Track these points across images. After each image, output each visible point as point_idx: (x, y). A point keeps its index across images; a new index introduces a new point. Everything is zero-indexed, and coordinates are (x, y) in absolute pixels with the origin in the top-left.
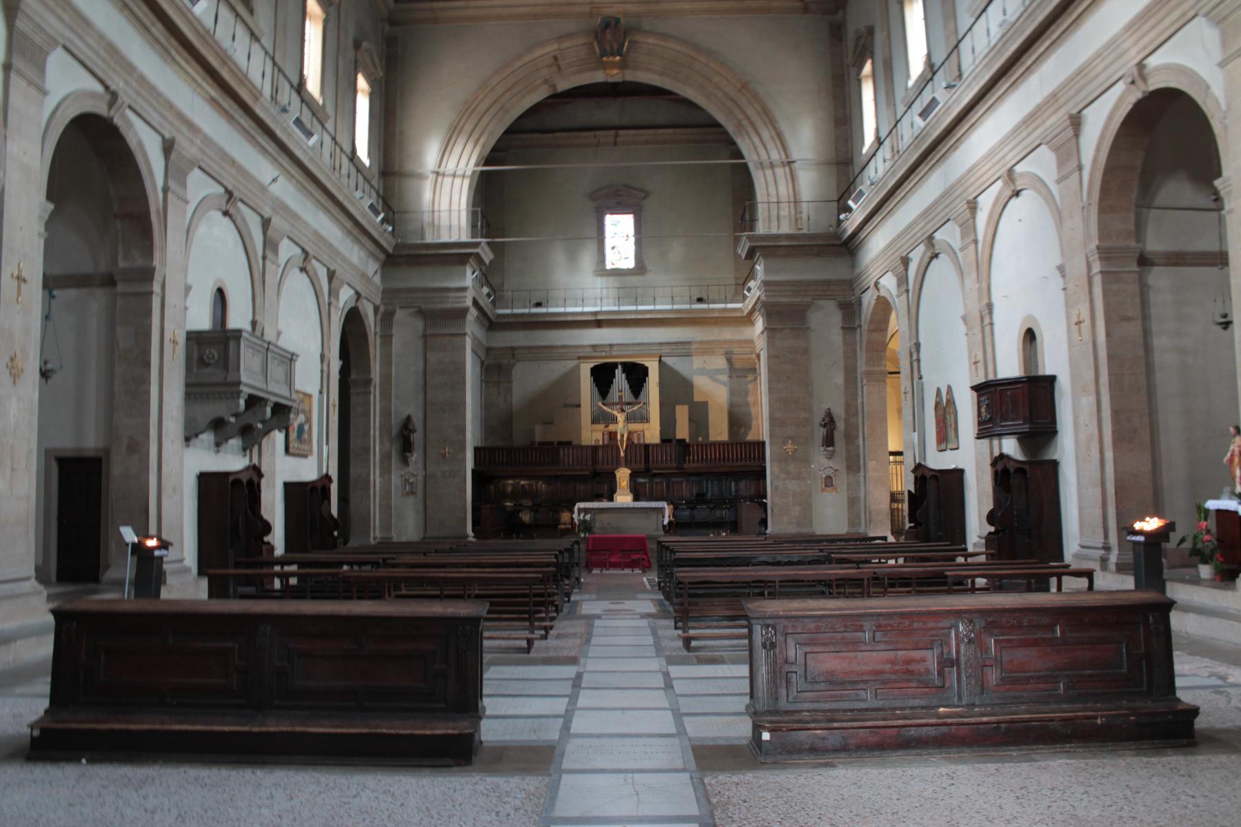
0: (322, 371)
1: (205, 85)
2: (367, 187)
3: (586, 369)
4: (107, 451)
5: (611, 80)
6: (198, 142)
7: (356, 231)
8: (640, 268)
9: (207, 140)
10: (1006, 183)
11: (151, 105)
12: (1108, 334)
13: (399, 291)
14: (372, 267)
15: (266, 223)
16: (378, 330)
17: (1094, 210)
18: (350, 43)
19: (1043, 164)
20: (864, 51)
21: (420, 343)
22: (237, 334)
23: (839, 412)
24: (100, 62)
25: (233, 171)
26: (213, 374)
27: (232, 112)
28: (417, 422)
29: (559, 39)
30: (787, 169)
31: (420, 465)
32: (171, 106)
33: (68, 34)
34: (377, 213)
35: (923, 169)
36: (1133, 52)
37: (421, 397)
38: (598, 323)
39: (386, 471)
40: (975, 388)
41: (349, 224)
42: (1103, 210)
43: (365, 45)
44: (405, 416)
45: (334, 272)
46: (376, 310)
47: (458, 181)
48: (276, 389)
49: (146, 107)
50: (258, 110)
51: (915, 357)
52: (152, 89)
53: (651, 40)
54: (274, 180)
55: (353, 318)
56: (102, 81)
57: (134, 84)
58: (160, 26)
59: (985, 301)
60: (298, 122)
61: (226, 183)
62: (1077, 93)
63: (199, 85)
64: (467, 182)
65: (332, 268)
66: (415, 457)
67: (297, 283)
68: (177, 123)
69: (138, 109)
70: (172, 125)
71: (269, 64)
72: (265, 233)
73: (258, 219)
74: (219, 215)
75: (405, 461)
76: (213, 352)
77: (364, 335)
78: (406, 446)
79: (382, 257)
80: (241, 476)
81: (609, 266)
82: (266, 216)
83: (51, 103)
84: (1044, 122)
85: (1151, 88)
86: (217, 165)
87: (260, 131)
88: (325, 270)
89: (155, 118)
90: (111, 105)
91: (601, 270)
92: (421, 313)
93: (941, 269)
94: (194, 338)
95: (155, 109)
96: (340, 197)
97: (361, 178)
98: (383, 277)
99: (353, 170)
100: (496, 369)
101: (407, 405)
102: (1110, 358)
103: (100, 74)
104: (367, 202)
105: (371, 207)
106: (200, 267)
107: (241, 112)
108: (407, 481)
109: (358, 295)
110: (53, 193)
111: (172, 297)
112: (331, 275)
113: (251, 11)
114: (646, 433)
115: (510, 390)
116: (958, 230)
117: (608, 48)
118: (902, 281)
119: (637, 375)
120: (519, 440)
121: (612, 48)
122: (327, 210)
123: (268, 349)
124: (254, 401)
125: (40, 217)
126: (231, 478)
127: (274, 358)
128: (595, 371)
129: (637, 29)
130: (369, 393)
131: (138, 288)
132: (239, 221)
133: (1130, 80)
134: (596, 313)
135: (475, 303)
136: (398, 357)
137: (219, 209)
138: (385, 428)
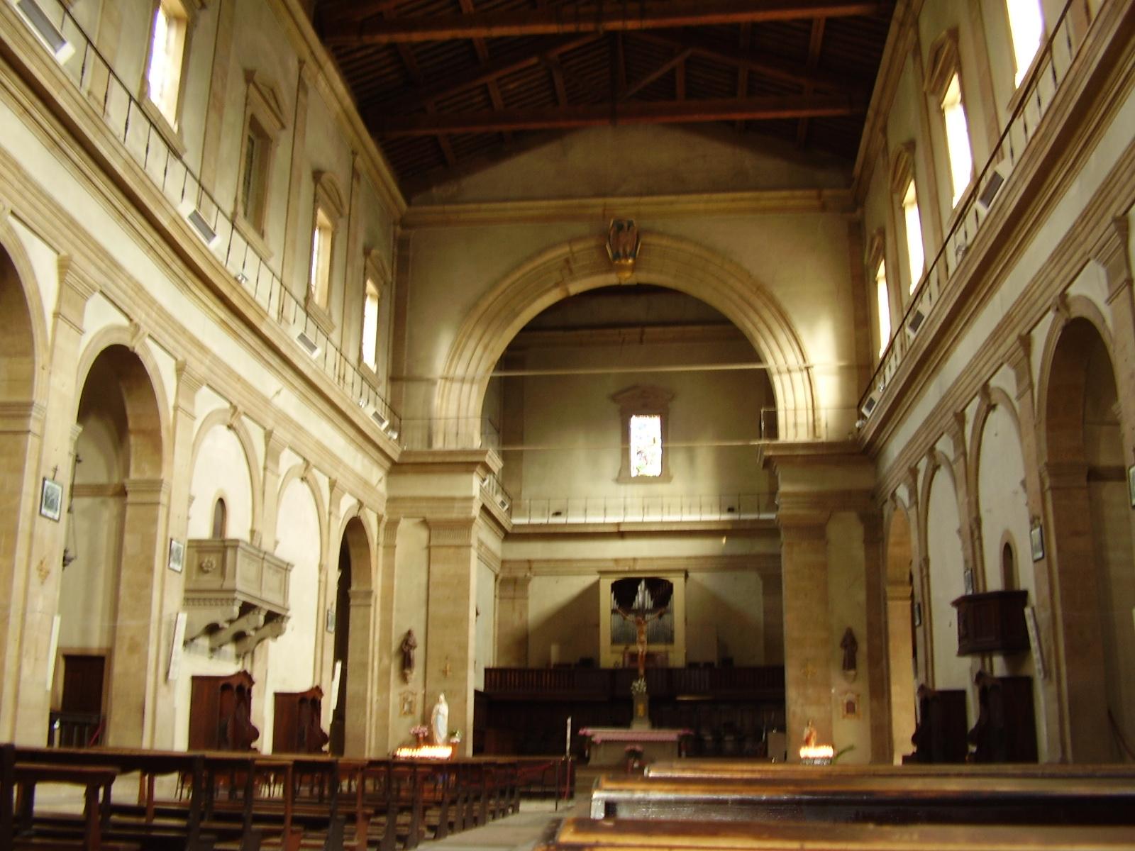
0: (320, 581)
1: (215, 309)
2: (372, 393)
3: (606, 585)
4: (111, 651)
5: (623, 283)
6: (207, 362)
7: (360, 440)
8: (665, 476)
9: (216, 360)
10: (982, 399)
11: (167, 332)
12: (1059, 549)
13: (403, 499)
14: (376, 475)
15: (268, 435)
16: (382, 539)
17: (1043, 427)
18: (360, 250)
19: (1005, 380)
20: (881, 252)
21: (424, 554)
22: (235, 544)
23: (861, 632)
24: (127, 300)
25: (239, 386)
26: (210, 581)
27: (239, 331)
28: (419, 638)
29: (571, 241)
30: (805, 373)
31: (421, 684)
32: (183, 330)
33: (103, 279)
34: (382, 421)
35: (921, 378)
36: (1058, 281)
37: (423, 611)
38: (620, 534)
39: (384, 687)
40: (957, 603)
41: (352, 432)
42: (1051, 427)
43: (374, 252)
44: (405, 630)
45: (335, 481)
46: (380, 519)
47: (466, 387)
48: (269, 597)
49: (163, 333)
50: (265, 330)
51: (925, 573)
52: (169, 318)
53: (664, 242)
54: (278, 393)
55: (355, 527)
56: (127, 315)
57: (154, 314)
58: (179, 263)
59: (974, 515)
60: (302, 337)
61: (230, 398)
62: (1025, 315)
63: (211, 310)
64: (475, 388)
65: (333, 477)
66: (416, 673)
67: (298, 494)
68: (189, 346)
69: (155, 336)
70: (184, 348)
71: (277, 285)
72: (267, 444)
73: (261, 432)
74: (224, 428)
75: (404, 678)
76: (213, 560)
77: (366, 545)
78: (406, 662)
79: (387, 464)
80: (231, 681)
81: (634, 473)
82: (268, 428)
83: (86, 340)
84: (1005, 341)
85: (1073, 316)
86: (221, 379)
87: (265, 348)
88: (327, 480)
89: (170, 343)
90: (134, 335)
91: (623, 476)
92: (425, 523)
93: (942, 480)
94: (197, 546)
95: (170, 335)
96: (343, 407)
97: (365, 386)
98: (389, 485)
99: (358, 379)
100: (511, 583)
101: (409, 618)
102: (1061, 572)
103: (126, 310)
104: (370, 410)
105: (376, 414)
106: (204, 471)
107: (248, 331)
108: (405, 700)
109: (361, 505)
110: (83, 415)
111: (178, 507)
112: (333, 485)
113: (262, 234)
114: (671, 656)
115: (525, 606)
116: (1102, 272)
117: (621, 251)
118: (913, 492)
119: (661, 589)
120: (533, 662)
121: (625, 251)
122: (330, 420)
123: (262, 557)
124: (247, 608)
125: (71, 439)
126: (221, 683)
127: (269, 568)
128: (616, 587)
129: (650, 232)
130: (369, 606)
131: (147, 498)
132: (242, 433)
133: (1055, 308)
134: (618, 524)
135: (484, 508)
136: (399, 571)
137: (223, 424)
138: (386, 642)
